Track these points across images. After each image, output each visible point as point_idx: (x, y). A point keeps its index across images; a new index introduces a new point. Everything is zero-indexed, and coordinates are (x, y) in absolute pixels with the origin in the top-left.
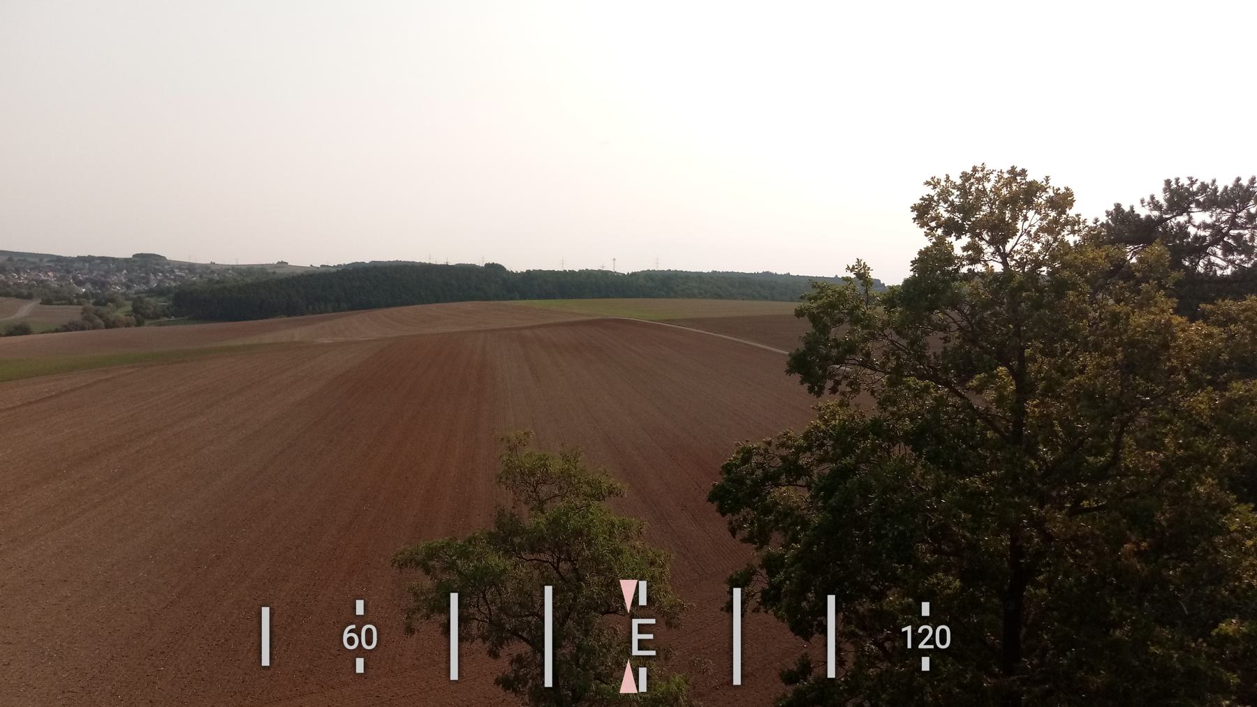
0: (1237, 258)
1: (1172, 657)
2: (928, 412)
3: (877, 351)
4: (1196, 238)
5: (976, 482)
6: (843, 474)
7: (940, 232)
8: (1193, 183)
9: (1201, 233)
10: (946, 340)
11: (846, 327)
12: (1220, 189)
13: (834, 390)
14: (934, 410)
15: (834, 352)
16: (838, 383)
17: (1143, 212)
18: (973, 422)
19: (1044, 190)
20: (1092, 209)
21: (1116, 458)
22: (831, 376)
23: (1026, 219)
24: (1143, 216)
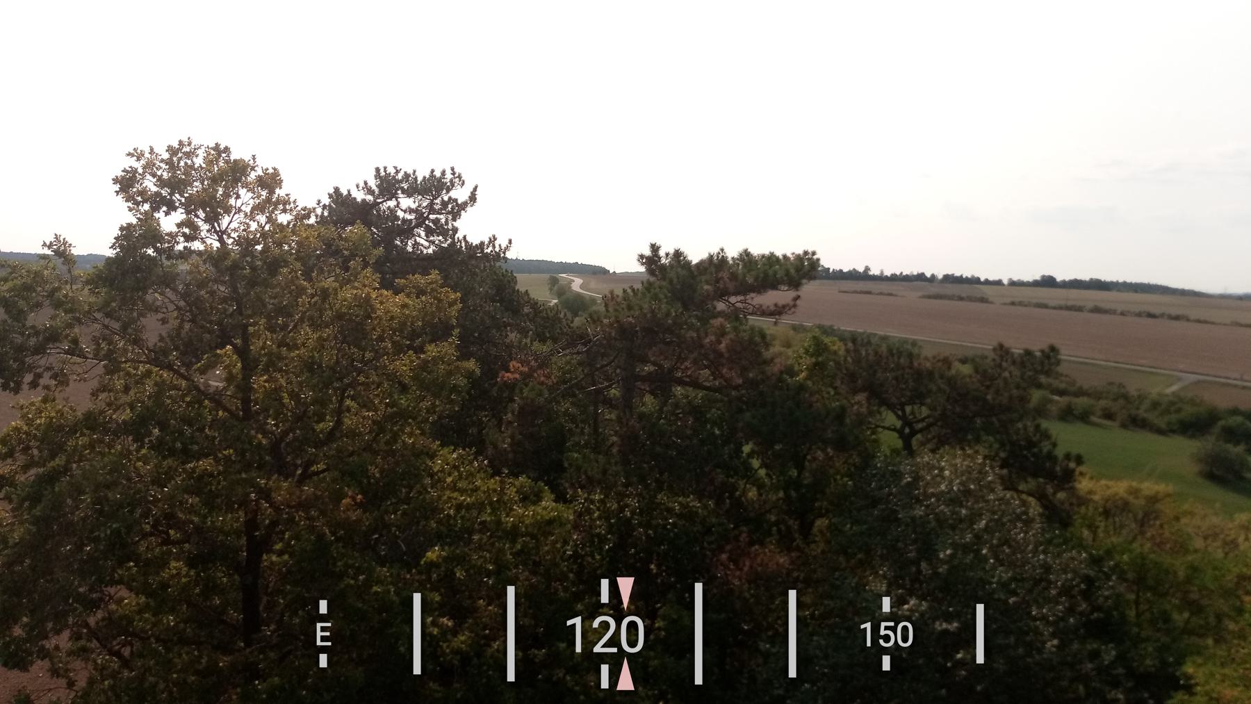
0: (437, 239)
1: (389, 592)
2: (149, 397)
3: (85, 335)
4: (404, 221)
5: (205, 464)
6: (51, 478)
7: (147, 207)
8: (397, 172)
9: (408, 217)
10: (164, 321)
11: (48, 311)
12: (420, 179)
13: (34, 385)
14: (158, 396)
15: (32, 341)
16: (39, 376)
17: (359, 196)
18: (200, 403)
19: (253, 169)
20: (308, 190)
21: (339, 423)
22: (30, 368)
23: (238, 197)
24: (359, 200)
